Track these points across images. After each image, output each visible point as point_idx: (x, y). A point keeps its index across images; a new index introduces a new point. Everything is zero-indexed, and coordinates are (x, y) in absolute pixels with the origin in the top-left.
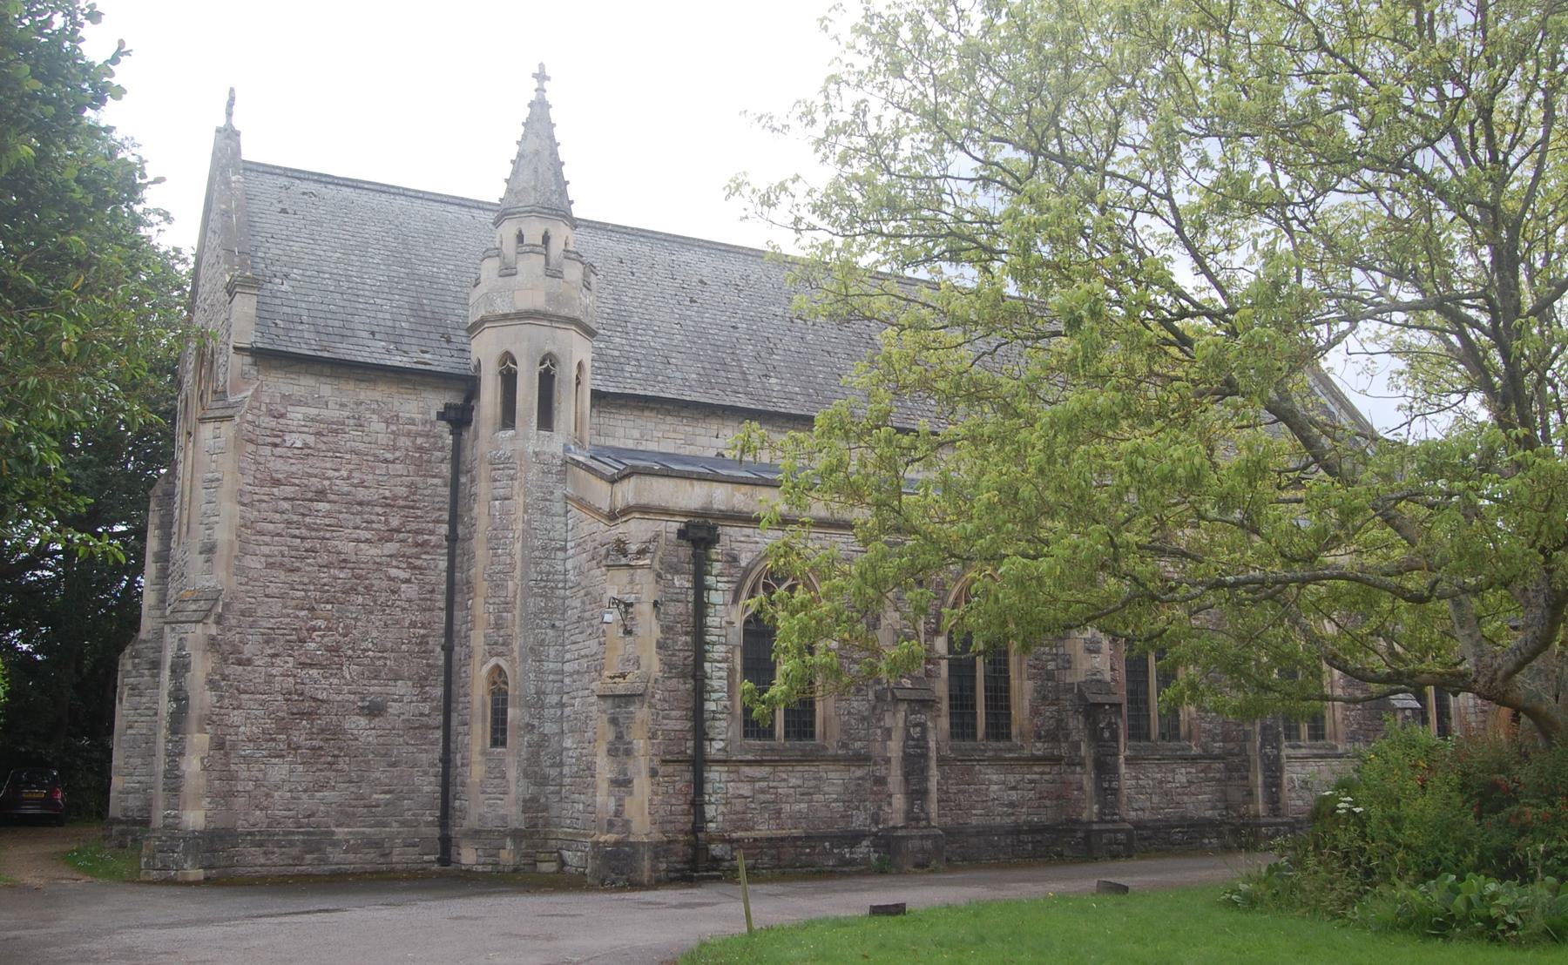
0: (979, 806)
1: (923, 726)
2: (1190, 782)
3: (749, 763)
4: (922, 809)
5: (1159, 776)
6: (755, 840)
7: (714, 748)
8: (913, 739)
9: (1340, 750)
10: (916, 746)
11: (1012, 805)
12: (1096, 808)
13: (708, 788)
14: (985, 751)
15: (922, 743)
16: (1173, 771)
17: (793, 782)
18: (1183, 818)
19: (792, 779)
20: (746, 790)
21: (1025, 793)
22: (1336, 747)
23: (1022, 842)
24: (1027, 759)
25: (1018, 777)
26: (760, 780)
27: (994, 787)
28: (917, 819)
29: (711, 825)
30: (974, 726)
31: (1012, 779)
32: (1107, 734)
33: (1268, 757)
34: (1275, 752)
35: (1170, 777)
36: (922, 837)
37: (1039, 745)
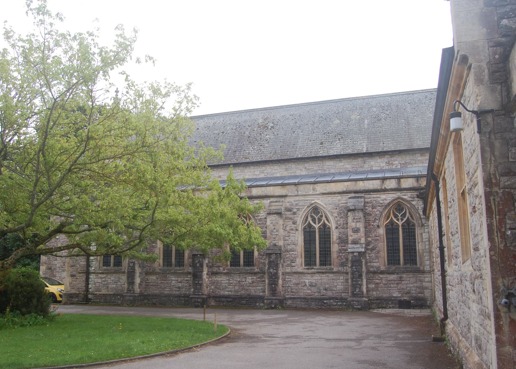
0: (168, 288)
1: (134, 263)
2: (253, 282)
3: (100, 273)
4: (132, 288)
5: (239, 279)
6: (100, 294)
7: (92, 269)
8: (131, 267)
9: (335, 270)
10: (131, 269)
11: (179, 288)
12: (192, 290)
13: (90, 280)
14: (171, 270)
15: (133, 268)
16: (246, 278)
17: (112, 279)
18: (249, 295)
19: (112, 278)
20: (100, 281)
21: (184, 284)
22: (333, 269)
23: (181, 300)
24: (186, 273)
25: (182, 279)
26: (103, 278)
27: (174, 282)
28: (130, 291)
29: (91, 290)
30: (399, 260)
31: (180, 279)
32: (198, 265)
33: (271, 273)
34: (275, 271)
35: (244, 280)
36: (130, 296)
37: (190, 268)
